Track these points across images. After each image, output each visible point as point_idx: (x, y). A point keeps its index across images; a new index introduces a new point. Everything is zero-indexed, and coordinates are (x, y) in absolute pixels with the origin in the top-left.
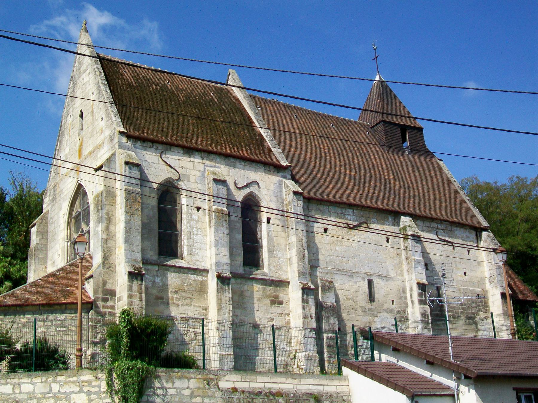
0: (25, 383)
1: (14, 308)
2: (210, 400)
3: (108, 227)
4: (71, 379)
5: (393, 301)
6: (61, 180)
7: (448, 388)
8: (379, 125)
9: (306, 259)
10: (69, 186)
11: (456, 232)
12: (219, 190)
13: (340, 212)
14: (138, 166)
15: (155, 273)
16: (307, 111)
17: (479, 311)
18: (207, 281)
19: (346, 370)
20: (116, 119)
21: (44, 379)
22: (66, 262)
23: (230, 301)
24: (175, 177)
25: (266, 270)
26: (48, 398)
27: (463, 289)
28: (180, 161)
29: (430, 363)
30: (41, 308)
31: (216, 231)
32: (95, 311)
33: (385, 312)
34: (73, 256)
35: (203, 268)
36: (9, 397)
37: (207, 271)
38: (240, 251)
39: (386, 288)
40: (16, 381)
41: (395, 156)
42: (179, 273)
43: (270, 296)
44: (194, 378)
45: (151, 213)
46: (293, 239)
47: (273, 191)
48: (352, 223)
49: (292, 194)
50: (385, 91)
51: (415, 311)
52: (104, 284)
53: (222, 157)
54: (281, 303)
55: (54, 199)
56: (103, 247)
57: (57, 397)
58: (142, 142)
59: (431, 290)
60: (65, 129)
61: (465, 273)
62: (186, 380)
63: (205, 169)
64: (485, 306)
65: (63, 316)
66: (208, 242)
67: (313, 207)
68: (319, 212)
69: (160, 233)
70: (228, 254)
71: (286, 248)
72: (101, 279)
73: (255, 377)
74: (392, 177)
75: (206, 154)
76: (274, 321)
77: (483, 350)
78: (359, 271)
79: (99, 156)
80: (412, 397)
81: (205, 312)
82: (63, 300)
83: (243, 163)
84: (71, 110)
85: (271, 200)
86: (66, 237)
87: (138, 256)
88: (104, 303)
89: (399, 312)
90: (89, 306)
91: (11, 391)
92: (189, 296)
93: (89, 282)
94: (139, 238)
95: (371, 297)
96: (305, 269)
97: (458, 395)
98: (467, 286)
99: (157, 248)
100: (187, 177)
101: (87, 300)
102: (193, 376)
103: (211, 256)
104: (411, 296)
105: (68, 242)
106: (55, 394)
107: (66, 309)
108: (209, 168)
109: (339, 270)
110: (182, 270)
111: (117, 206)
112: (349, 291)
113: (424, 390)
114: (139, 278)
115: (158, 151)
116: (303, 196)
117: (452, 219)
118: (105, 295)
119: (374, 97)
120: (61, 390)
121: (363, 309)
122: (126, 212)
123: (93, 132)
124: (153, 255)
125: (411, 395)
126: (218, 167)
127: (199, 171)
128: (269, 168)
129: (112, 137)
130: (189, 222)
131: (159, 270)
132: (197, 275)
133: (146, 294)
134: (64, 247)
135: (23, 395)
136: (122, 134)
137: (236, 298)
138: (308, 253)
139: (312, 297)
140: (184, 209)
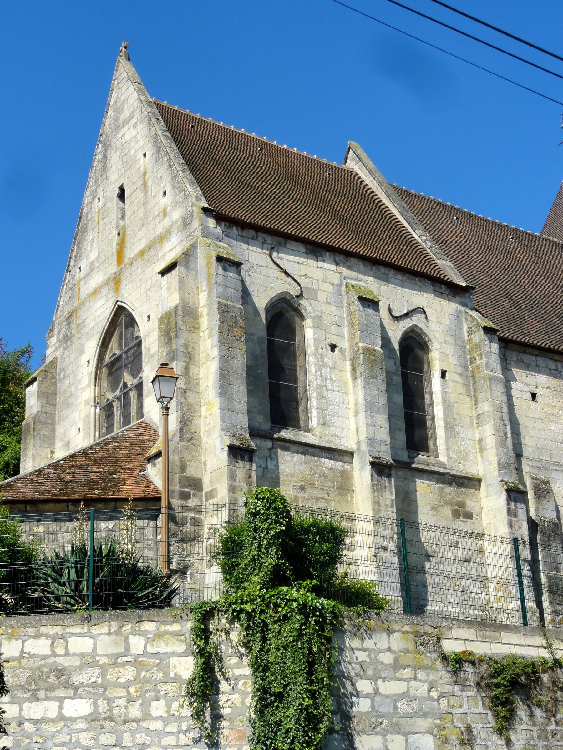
0: (75, 635)
2: (428, 675)
4: (169, 628)
6: (83, 304)
10: (98, 313)
12: (368, 315)
13: (554, 367)
14: (237, 265)
15: (266, 452)
18: (351, 471)
20: (193, 190)
21: (114, 626)
23: (392, 506)
24: (294, 291)
25: (442, 458)
26: (123, 665)
28: (302, 266)
31: (367, 385)
34: (104, 430)
35: (341, 448)
36: (43, 662)
37: (352, 454)
40: (58, 630)
42: (305, 454)
43: (450, 503)
44: (398, 631)
45: (258, 350)
46: (486, 407)
49: (482, 332)
52: (183, 468)
54: (469, 516)
55: (67, 338)
57: (141, 664)
58: (239, 228)
60: (88, 221)
62: (385, 635)
63: (341, 281)
65: (110, 524)
67: (513, 356)
68: (522, 364)
71: (472, 423)
73: (498, 634)
79: (160, 255)
82: (110, 495)
83: (400, 277)
84: (100, 189)
85: (445, 341)
87: (243, 420)
88: (182, 502)
92: (322, 496)
96: (509, 459)
100: (314, 293)
105: (96, 407)
110: (311, 450)
111: (202, 334)
115: (265, 246)
118: (184, 486)
120: (150, 650)
122: (222, 343)
123: (145, 217)
127: (332, 284)
128: (441, 288)
129: (189, 221)
130: (319, 369)
131: (273, 448)
132: (335, 459)
134: (87, 416)
136: (208, 213)
138: (512, 433)
140: (310, 348)
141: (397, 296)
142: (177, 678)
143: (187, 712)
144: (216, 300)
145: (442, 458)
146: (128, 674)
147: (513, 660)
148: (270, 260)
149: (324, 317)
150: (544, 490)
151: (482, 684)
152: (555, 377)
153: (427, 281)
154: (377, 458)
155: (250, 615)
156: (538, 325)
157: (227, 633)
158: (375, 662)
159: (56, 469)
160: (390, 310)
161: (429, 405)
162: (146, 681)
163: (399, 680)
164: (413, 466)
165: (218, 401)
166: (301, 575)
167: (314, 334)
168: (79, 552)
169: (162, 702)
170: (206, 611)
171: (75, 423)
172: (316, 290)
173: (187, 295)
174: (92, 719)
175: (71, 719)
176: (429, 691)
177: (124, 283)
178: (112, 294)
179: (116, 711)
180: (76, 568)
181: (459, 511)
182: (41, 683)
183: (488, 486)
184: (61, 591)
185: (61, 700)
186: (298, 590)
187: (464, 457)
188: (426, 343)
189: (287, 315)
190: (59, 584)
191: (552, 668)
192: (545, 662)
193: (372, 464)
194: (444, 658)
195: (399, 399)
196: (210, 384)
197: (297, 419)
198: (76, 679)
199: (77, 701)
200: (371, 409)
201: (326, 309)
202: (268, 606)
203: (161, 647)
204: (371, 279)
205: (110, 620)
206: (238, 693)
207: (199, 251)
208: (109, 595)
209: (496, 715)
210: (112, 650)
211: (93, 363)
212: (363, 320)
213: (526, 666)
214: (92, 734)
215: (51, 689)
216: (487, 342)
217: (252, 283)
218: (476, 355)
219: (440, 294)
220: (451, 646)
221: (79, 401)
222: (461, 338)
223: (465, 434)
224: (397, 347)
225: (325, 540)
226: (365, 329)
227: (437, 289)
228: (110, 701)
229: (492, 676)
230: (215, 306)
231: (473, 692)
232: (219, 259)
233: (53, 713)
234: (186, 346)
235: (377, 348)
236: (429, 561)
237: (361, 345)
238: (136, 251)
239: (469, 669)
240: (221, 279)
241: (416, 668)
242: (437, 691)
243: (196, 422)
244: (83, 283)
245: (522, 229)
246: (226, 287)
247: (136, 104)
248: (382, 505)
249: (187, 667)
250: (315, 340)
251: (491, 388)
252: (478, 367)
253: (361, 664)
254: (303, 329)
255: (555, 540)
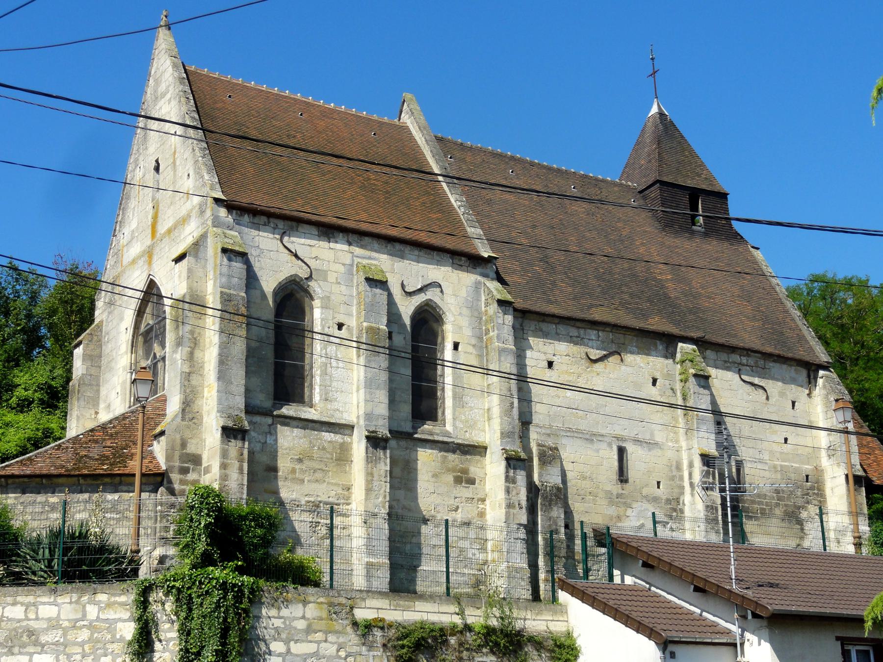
0: (44, 603)
2: (338, 638)
3: (191, 354)
4: (117, 599)
5: (659, 483)
6: (123, 272)
7: (729, 632)
8: (652, 189)
9: (515, 412)
11: (773, 370)
12: (375, 295)
13: (576, 334)
15: (266, 428)
16: (532, 164)
17: (808, 503)
18: (351, 443)
19: (563, 596)
20: (210, 178)
21: (75, 597)
22: (127, 406)
23: (386, 476)
24: (303, 273)
25: (449, 427)
26: (81, 628)
27: (781, 466)
28: (313, 249)
29: (702, 589)
30: (81, 481)
32: (167, 489)
33: (644, 500)
35: (343, 422)
36: (18, 625)
39: (647, 460)
40: (31, 599)
41: (678, 241)
42: (304, 428)
43: (453, 470)
48: (595, 354)
49: (496, 305)
50: (666, 128)
52: (184, 445)
53: (383, 242)
54: (472, 482)
57: (95, 627)
59: (722, 468)
61: (786, 440)
62: (301, 605)
63: (353, 261)
64: (817, 494)
65: (116, 496)
67: (531, 325)
68: (541, 333)
69: (276, 364)
70: (386, 400)
72: (178, 437)
74: (669, 277)
76: (460, 510)
77: (797, 571)
78: (603, 432)
80: (665, 645)
81: (346, 493)
82: (116, 471)
83: (416, 252)
84: (141, 158)
86: (129, 365)
87: (240, 402)
88: (182, 476)
89: (668, 501)
90: (156, 480)
91: (22, 616)
93: (159, 442)
94: (242, 373)
95: (622, 476)
96: (513, 428)
97: (742, 644)
98: (789, 461)
99: (271, 388)
100: (324, 275)
101: (155, 471)
103: (358, 403)
104: (690, 475)
105: (132, 373)
106: (91, 622)
107: (120, 483)
108: (360, 260)
109: (570, 430)
110: (311, 425)
112: (585, 466)
114: (239, 436)
115: (277, 231)
116: (515, 310)
117: (769, 349)
119: (648, 141)
120: (102, 616)
124: (263, 400)
125: (662, 641)
126: (374, 259)
127: (344, 265)
128: (460, 260)
131: (273, 424)
134: (124, 382)
135: (41, 622)
137: (398, 471)
139: (523, 473)
141: (406, 273)
142: (122, 639)
144: (219, 290)
145: (449, 427)
146: (84, 635)
147: (422, 625)
148: (280, 245)
149: (333, 297)
150: (550, 456)
151: (389, 645)
152: (576, 344)
153: (445, 254)
154: (373, 432)
156: (570, 289)
157: (163, 604)
158: (289, 628)
159: (74, 444)
161: (441, 376)
162: (98, 641)
163: (311, 642)
164: (416, 436)
166: (227, 557)
167: (322, 314)
169: (110, 657)
170: (146, 587)
171: (115, 387)
172: (326, 271)
173: (195, 284)
176: (338, 651)
177: (155, 258)
180: (50, 549)
181: (461, 477)
183: (492, 453)
184: (36, 566)
186: (222, 571)
188: (440, 316)
189: (298, 296)
190: (36, 561)
191: (461, 632)
192: (455, 626)
193: (367, 437)
194: (355, 624)
196: (212, 368)
198: (43, 639)
199: (44, 656)
200: (370, 385)
201: (336, 289)
202: (194, 583)
203: (111, 615)
204: (385, 256)
205: (72, 591)
207: (209, 240)
208: (75, 571)
210: (72, 616)
211: (131, 331)
213: (432, 631)
215: (23, 646)
216: (501, 315)
218: (490, 326)
219: (459, 267)
220: (362, 614)
221: (119, 366)
224: (407, 321)
226: (370, 309)
229: (399, 639)
230: (219, 295)
231: (379, 652)
232: (224, 251)
235: (381, 327)
236: (426, 524)
237: (365, 324)
239: (378, 633)
240: (225, 270)
241: (327, 632)
242: (346, 651)
243: (199, 402)
244: (125, 249)
245: (591, 175)
246: (230, 276)
247: (170, 79)
248: (375, 475)
249: (129, 630)
250: (322, 320)
251: (499, 360)
252: (491, 338)
253: (276, 629)
254: (312, 308)
255: (556, 504)
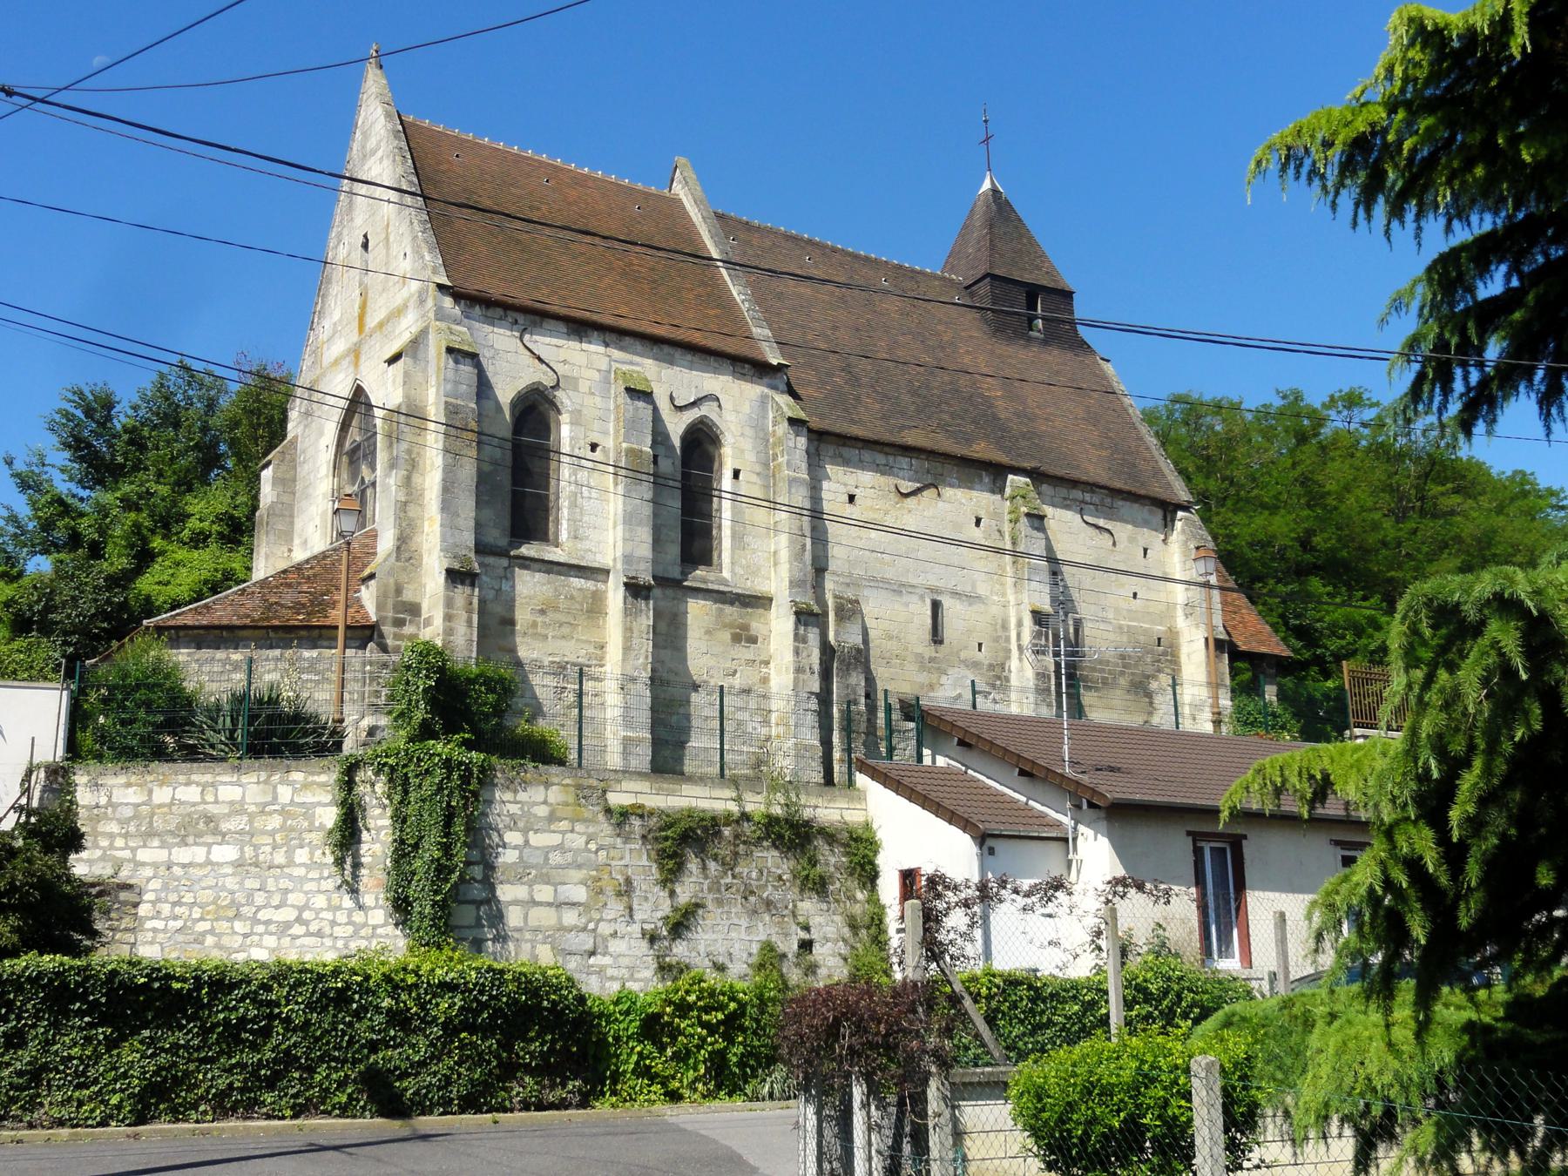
0: (225, 783)
1: (217, 632)
3: (408, 479)
4: (316, 778)
5: (980, 645)
6: (323, 374)
7: (1059, 824)
12: (637, 409)
15: (501, 572)
17: (1159, 671)
18: (606, 592)
19: (861, 779)
20: (432, 259)
21: (263, 776)
24: (548, 380)
25: (726, 574)
26: (270, 813)
29: (1029, 773)
30: (271, 634)
35: (596, 565)
37: (607, 572)
38: (676, 535)
40: (208, 778)
41: (1011, 350)
42: (548, 572)
43: (731, 626)
47: (744, 415)
48: (907, 486)
49: (786, 424)
50: (1000, 206)
51: (1023, 671)
52: (399, 591)
54: (753, 640)
56: (398, 518)
59: (1057, 627)
61: (1135, 595)
65: (315, 653)
66: (611, 516)
72: (392, 581)
75: (614, 337)
78: (914, 581)
83: (689, 357)
84: (345, 232)
87: (469, 539)
89: (991, 667)
90: (364, 634)
94: (471, 503)
95: (936, 636)
97: (1075, 839)
99: (507, 523)
100: (574, 382)
102: (556, 780)
107: (320, 637)
109: (874, 579)
110: (556, 568)
112: (892, 623)
113: (1008, 826)
121: (919, 656)
122: (446, 451)
124: (496, 536)
132: (586, 578)
133: (481, 613)
137: (663, 626)
141: (677, 384)
143: (330, 859)
145: (726, 574)
146: (275, 822)
147: (690, 813)
149: (585, 412)
152: (883, 474)
155: (393, 769)
156: (878, 406)
157: (373, 785)
158: (527, 814)
160: (672, 398)
162: (292, 829)
165: (438, 517)
166: (451, 728)
168: (239, 700)
174: (238, 864)
175: (217, 864)
177: (363, 358)
178: (351, 369)
179: (261, 858)
182: (190, 829)
185: (209, 845)
187: (753, 571)
191: (737, 822)
193: (626, 584)
194: (608, 811)
195: (675, 503)
197: (546, 533)
198: (224, 826)
201: (589, 401)
202: (411, 760)
203: (308, 798)
205: (260, 769)
206: (377, 842)
209: (661, 867)
211: (332, 450)
212: (629, 415)
213: (702, 820)
214: (238, 879)
215: (199, 835)
217: (496, 373)
219: (742, 376)
220: (616, 799)
222: (764, 429)
223: (756, 547)
224: (677, 443)
225: (491, 690)
227: (738, 369)
228: (256, 847)
229: (661, 829)
230: (442, 407)
232: (450, 350)
233: (201, 858)
234: (409, 452)
238: (377, 320)
239: (636, 822)
240: (450, 374)
243: (417, 539)
246: (457, 383)
249: (330, 816)
250: (572, 439)
253: (512, 816)
254: (558, 424)
